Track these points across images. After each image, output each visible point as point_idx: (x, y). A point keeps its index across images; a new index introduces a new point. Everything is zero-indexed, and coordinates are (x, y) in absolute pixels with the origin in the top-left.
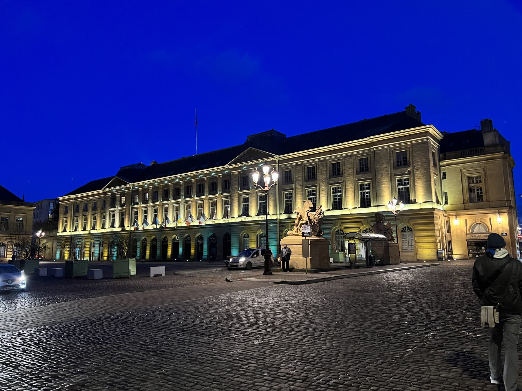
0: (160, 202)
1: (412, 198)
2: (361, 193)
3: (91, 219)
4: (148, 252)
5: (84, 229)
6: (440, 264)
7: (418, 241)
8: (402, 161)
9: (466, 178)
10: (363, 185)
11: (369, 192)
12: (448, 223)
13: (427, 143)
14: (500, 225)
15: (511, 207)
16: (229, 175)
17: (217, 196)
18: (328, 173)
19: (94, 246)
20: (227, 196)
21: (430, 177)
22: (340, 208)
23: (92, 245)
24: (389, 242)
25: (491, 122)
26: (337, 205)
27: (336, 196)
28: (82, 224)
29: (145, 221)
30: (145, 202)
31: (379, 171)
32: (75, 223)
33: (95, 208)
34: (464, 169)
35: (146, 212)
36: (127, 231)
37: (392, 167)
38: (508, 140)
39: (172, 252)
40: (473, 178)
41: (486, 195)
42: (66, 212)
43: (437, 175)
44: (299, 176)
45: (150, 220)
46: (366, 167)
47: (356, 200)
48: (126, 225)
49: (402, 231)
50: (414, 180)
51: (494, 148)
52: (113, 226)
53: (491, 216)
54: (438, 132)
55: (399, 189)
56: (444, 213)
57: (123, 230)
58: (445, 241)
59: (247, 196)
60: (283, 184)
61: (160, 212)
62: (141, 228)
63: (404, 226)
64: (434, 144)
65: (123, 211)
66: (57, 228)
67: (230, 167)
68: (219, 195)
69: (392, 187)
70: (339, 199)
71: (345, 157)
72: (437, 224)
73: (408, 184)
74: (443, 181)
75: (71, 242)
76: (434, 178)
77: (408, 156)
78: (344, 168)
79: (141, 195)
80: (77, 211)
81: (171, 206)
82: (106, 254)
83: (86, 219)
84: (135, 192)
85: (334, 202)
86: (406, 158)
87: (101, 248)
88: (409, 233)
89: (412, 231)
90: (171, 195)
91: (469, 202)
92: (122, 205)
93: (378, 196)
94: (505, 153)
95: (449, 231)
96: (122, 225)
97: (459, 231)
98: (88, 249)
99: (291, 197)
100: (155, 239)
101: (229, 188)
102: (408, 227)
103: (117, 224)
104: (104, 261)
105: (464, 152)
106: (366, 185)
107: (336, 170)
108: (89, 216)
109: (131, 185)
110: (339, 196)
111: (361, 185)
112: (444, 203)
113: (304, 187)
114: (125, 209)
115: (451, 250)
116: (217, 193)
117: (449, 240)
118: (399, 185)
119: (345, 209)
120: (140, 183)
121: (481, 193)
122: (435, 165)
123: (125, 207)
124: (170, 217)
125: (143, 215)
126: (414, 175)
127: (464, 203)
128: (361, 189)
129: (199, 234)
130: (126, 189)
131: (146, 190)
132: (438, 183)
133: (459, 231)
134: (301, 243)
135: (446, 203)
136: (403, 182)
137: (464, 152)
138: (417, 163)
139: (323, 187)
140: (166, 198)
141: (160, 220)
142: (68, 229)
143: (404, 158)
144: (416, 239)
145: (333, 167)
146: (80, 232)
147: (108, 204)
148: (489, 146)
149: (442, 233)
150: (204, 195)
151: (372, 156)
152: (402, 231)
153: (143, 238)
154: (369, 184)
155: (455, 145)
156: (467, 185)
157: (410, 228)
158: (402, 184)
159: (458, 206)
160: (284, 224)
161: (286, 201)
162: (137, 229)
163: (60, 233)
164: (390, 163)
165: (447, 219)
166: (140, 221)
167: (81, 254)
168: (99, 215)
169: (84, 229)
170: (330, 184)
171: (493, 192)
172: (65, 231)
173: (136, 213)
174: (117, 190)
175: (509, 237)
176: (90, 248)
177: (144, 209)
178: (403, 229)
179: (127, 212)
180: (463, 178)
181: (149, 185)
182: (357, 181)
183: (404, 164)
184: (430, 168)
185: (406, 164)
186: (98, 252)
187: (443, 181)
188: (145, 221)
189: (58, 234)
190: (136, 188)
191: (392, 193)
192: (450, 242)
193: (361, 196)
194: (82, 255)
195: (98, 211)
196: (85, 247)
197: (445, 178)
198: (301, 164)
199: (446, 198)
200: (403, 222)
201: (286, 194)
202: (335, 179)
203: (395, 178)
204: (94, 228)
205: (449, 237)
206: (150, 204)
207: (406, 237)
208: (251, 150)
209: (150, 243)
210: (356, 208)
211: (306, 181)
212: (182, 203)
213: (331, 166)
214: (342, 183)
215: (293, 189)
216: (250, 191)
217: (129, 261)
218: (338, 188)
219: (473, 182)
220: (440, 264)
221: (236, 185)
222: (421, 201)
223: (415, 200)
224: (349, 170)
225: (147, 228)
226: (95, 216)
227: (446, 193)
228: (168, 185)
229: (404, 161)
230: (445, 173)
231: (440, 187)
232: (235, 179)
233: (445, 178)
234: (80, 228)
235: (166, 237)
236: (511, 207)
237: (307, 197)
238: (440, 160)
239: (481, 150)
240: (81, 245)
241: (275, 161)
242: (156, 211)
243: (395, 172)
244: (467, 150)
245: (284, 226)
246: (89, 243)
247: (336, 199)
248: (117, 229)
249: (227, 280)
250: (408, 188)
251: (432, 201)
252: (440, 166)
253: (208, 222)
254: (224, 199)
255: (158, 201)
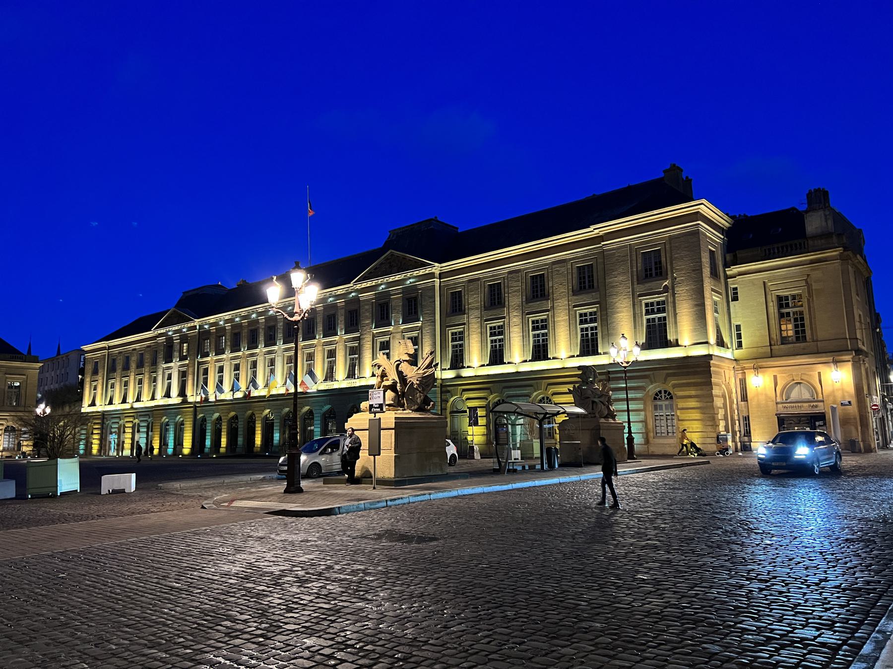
0: (244, 352)
1: (671, 337)
2: (582, 330)
3: (135, 383)
4: (224, 441)
5: (124, 401)
6: (708, 463)
7: (682, 417)
8: (652, 268)
9: (774, 299)
10: (585, 314)
11: (596, 327)
12: (743, 383)
13: (696, 234)
14: (838, 385)
15: (858, 352)
16: (356, 300)
17: (336, 338)
18: (524, 294)
19: (139, 431)
20: (354, 339)
21: (703, 298)
22: (546, 358)
23: (136, 429)
24: (602, 420)
25: (826, 194)
26: (540, 352)
27: (538, 335)
28: (120, 392)
29: (219, 388)
30: (220, 351)
31: (613, 287)
32: (110, 390)
33: (140, 365)
34: (770, 281)
35: (221, 370)
36: (190, 403)
37: (635, 280)
38: (857, 227)
39: (262, 441)
40: (787, 298)
41: (811, 329)
42: (95, 372)
43: (720, 293)
44: (474, 300)
45: (226, 386)
46: (589, 282)
47: (526, 339)
48: (189, 392)
49: (655, 399)
50: (674, 303)
51: (824, 240)
52: (168, 395)
53: (821, 368)
54: (720, 213)
55: (648, 320)
56: (734, 363)
57: (185, 401)
58: (736, 418)
59: (386, 338)
60: (448, 315)
61: (244, 369)
62: (212, 398)
63: (658, 389)
64: (715, 237)
65: (184, 369)
66: (80, 399)
67: (358, 287)
68: (341, 338)
69: (634, 317)
70: (543, 340)
71: (554, 263)
72: (718, 385)
73: (664, 311)
74: (732, 304)
75: (102, 424)
76: (711, 298)
77: (663, 259)
78: (550, 285)
79: (213, 340)
80: (112, 369)
81: (262, 358)
82: (156, 445)
83: (126, 384)
84: (204, 334)
85: (535, 347)
86: (660, 262)
87: (150, 433)
88: (667, 403)
89: (671, 398)
90: (262, 338)
91: (779, 343)
92: (182, 358)
93: (609, 333)
94: (846, 249)
95: (744, 398)
96: (182, 393)
97: (762, 398)
98: (130, 436)
99: (461, 339)
100: (235, 418)
101: (357, 324)
102: (665, 392)
103: (175, 391)
104: (168, 456)
105: (769, 250)
106: (591, 314)
107: (538, 290)
108: (132, 377)
109: (197, 322)
110: (543, 335)
111: (581, 315)
112: (735, 345)
113: (484, 320)
114: (187, 365)
115: (748, 433)
116: (336, 334)
117: (745, 414)
118: (647, 313)
119: (554, 358)
120: (212, 319)
121: (803, 325)
122: (714, 274)
123: (187, 362)
124: (260, 381)
125: (233, 373)
126: (674, 294)
127: (771, 345)
128: (581, 322)
129: (307, 408)
130: (190, 329)
131: (221, 331)
132: (722, 307)
133: (762, 398)
134: (367, 427)
135: (740, 345)
136: (655, 307)
137: (769, 250)
138: (680, 272)
139: (515, 320)
140: (253, 345)
141: (243, 385)
142: (98, 402)
143: (656, 263)
144: (678, 412)
145: (533, 283)
146: (117, 406)
147: (161, 356)
148: (815, 237)
149: (731, 402)
150: (315, 338)
151: (600, 260)
152: (655, 399)
153: (216, 415)
154: (595, 313)
155: (750, 239)
156: (776, 311)
157: (669, 394)
158: (653, 312)
159: (760, 350)
160: (449, 388)
161: (453, 346)
162: (206, 400)
163: (86, 409)
164: (632, 272)
165: (740, 376)
166: (211, 388)
167: (118, 445)
168: (147, 376)
169: (124, 401)
170: (528, 314)
171: (823, 326)
172: (93, 404)
173: (206, 372)
174: (175, 332)
175: (856, 410)
176: (133, 434)
177: (218, 364)
178: (657, 394)
179: (191, 370)
180: (769, 297)
181: (227, 321)
182: (575, 306)
183: (656, 274)
184: (702, 281)
185: (661, 274)
186: (144, 440)
187: (732, 304)
188: (219, 388)
189: (83, 410)
190: (206, 327)
191: (635, 327)
192: (747, 419)
193: (582, 335)
194: (120, 446)
195: (146, 369)
196: (124, 432)
197: (735, 299)
198: (478, 279)
199: (739, 336)
200: (655, 382)
201: (452, 334)
202: (536, 305)
203: (641, 301)
204: (138, 400)
205: (745, 410)
206: (227, 355)
207: (661, 409)
208: (392, 255)
209: (262, 423)
210: (573, 356)
211: (486, 309)
212: (280, 353)
213: (529, 280)
214: (548, 311)
215: (464, 324)
216: (391, 329)
217: (57, 464)
218: (542, 321)
219: (787, 305)
220: (708, 463)
221: (367, 318)
222: (686, 343)
223: (677, 340)
224: (560, 288)
225: (222, 397)
226: (140, 377)
227: (738, 328)
228: (256, 321)
229: (656, 269)
230: (736, 289)
231: (726, 317)
232: (367, 307)
233: (735, 299)
234: (117, 400)
235: (253, 414)
236: (858, 352)
237: (489, 339)
238: (727, 265)
239: (800, 244)
240: (119, 428)
241: (434, 273)
242: (237, 367)
243: (639, 289)
244: (776, 246)
245: (449, 391)
246: (130, 425)
247: (539, 341)
248: (175, 400)
249: (203, 507)
250: (665, 318)
251: (707, 343)
252: (727, 277)
253: (323, 386)
254: (349, 344)
255: (240, 350)
